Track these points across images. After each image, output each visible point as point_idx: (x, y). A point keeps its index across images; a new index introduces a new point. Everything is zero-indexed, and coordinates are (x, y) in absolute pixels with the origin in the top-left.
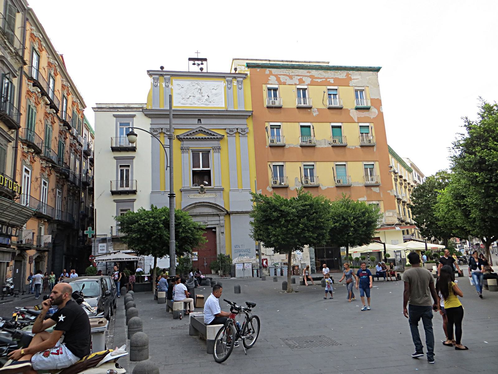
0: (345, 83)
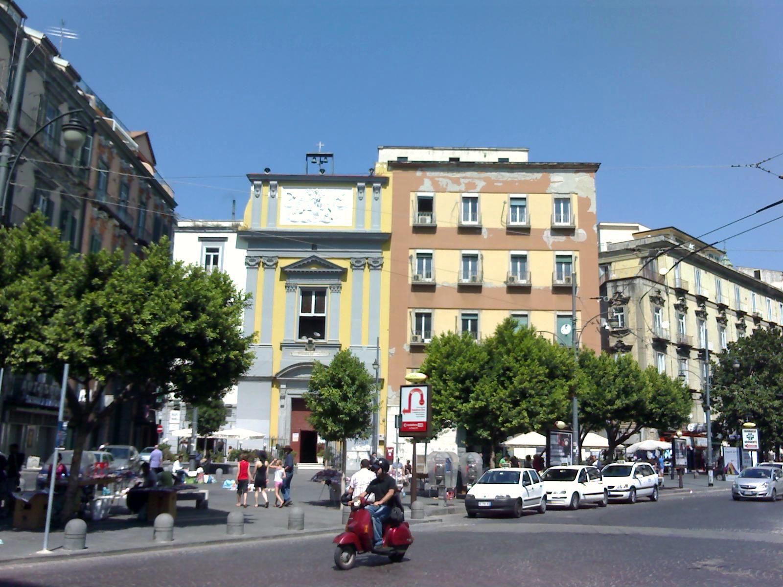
0: (541, 189)
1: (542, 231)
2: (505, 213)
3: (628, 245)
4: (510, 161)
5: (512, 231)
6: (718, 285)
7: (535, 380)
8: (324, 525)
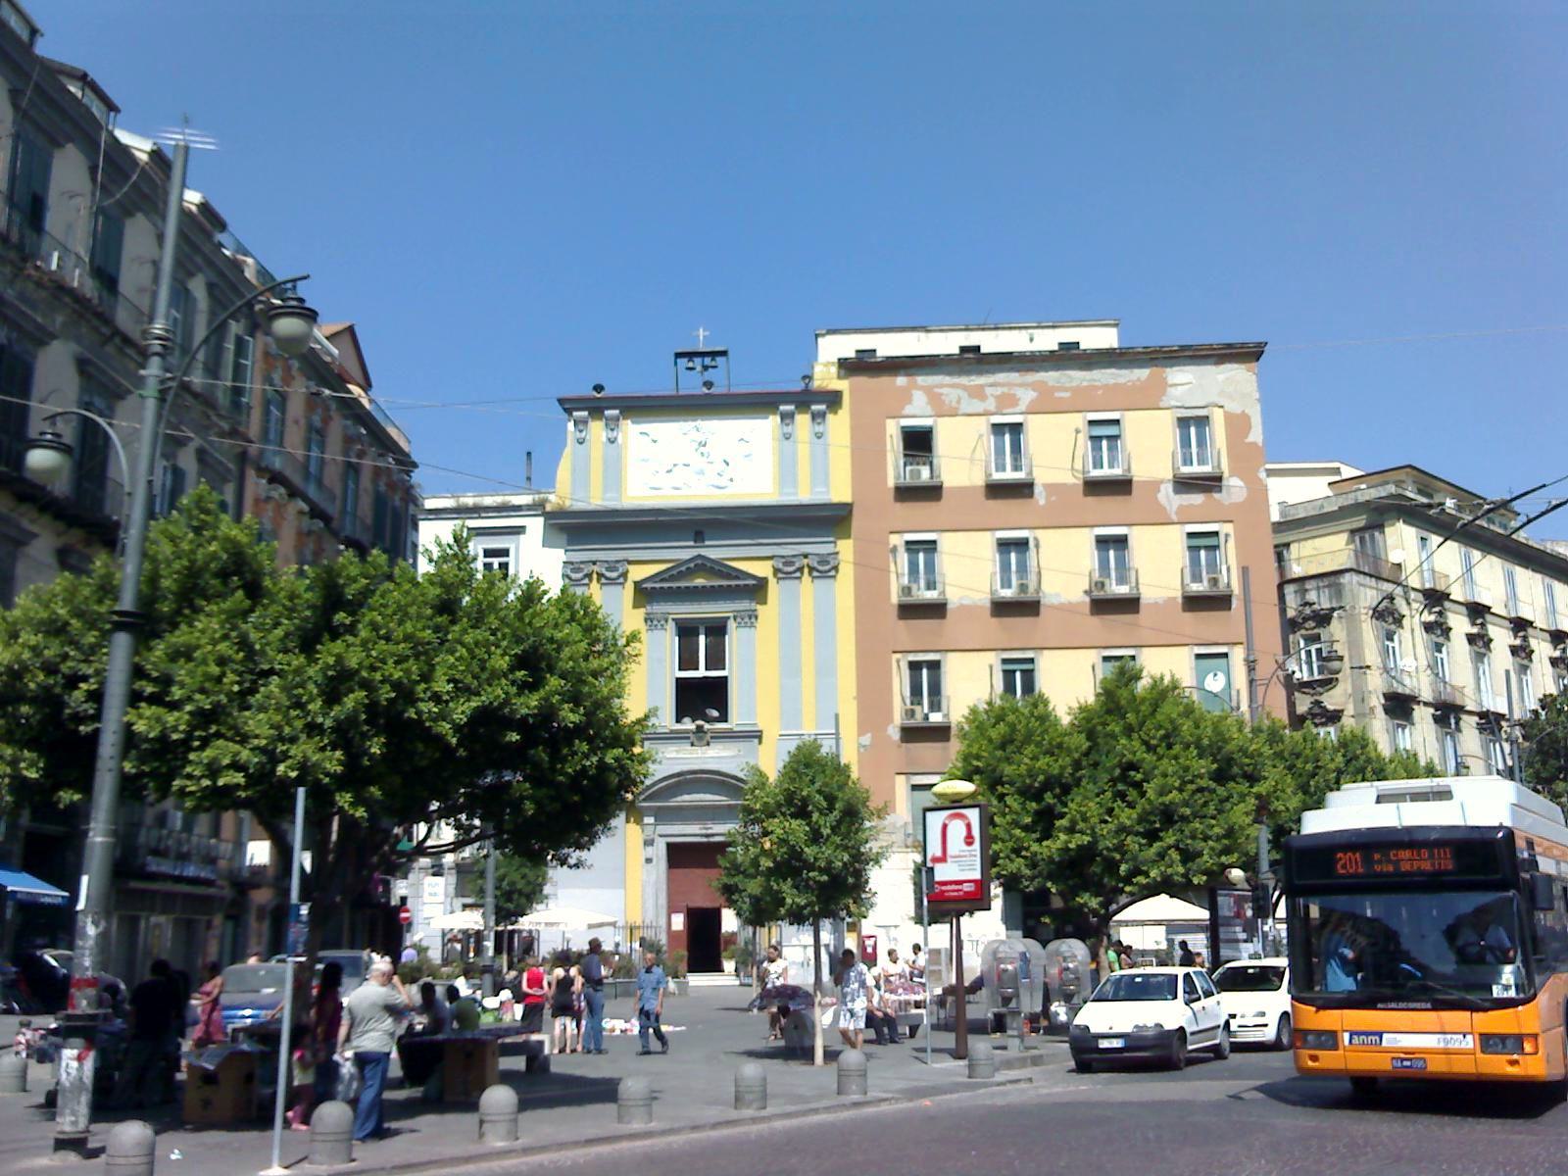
0: (1148, 400)
1: (1155, 485)
2: (1079, 453)
3: (1322, 507)
4: (1082, 346)
5: (1095, 487)
6: (1510, 579)
7: (1191, 787)
8: (801, 1099)
